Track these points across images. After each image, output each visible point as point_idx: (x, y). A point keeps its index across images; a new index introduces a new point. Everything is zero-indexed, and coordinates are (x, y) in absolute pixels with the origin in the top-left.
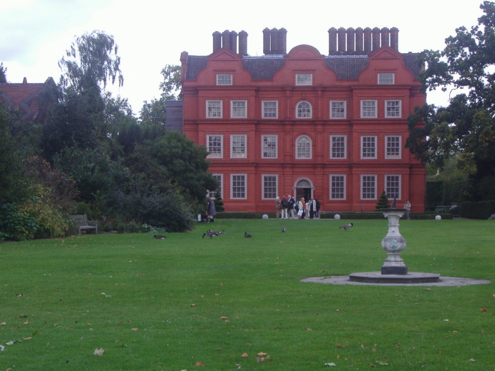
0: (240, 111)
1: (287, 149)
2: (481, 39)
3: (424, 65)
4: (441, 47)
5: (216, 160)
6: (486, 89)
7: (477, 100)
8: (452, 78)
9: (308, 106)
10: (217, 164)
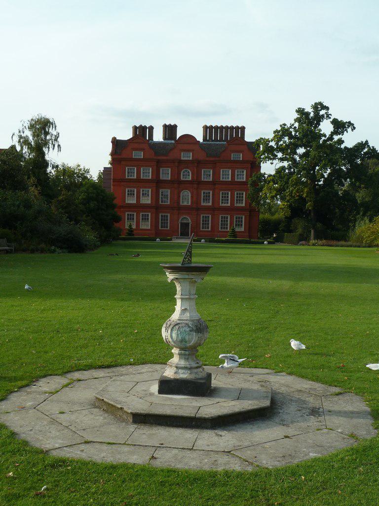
0: (148, 173)
1: (176, 199)
2: (296, 131)
3: (260, 147)
4: (271, 136)
5: (131, 204)
6: (298, 163)
7: (292, 170)
8: (277, 156)
9: (189, 172)
10: (130, 207)
